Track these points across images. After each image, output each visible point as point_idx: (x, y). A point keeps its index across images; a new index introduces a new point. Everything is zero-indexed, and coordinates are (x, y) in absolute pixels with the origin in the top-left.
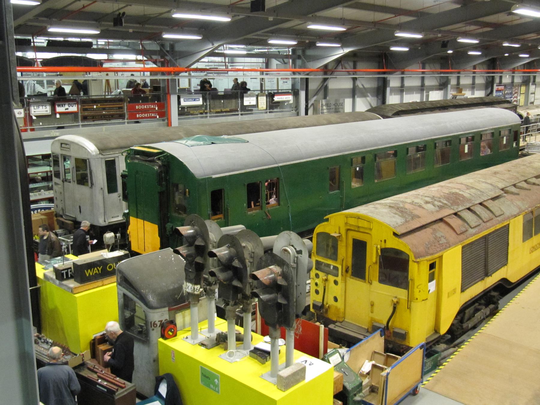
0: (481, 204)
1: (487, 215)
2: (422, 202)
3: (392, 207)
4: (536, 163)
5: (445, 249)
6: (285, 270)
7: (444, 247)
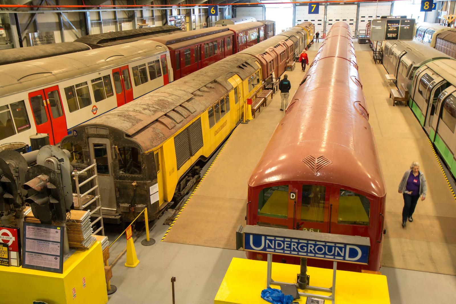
0: (180, 105)
1: (186, 113)
2: (141, 110)
3: (121, 116)
4: (210, 73)
5: (164, 141)
6: (52, 176)
7: (163, 140)
